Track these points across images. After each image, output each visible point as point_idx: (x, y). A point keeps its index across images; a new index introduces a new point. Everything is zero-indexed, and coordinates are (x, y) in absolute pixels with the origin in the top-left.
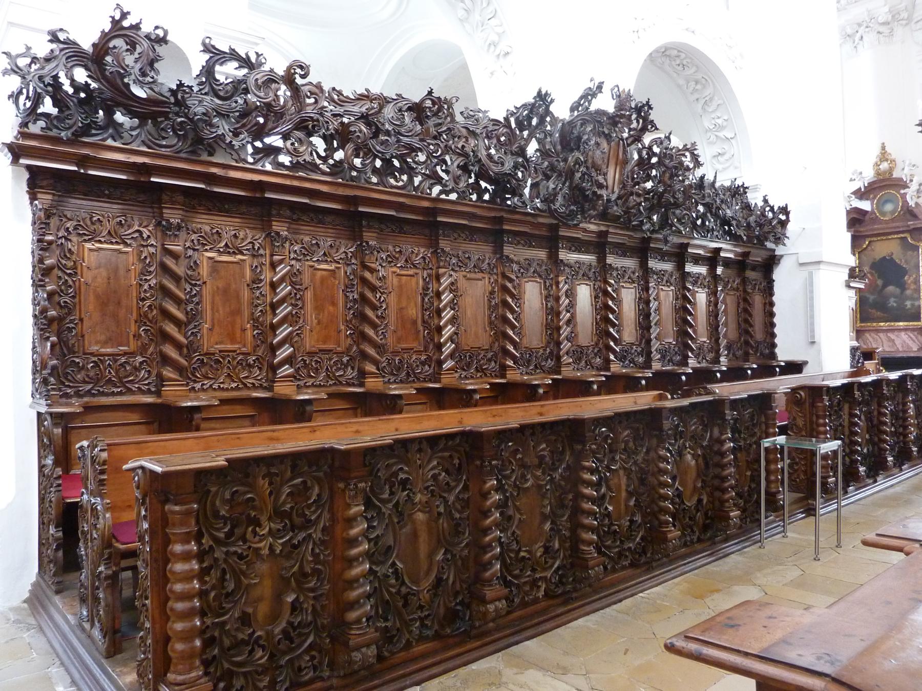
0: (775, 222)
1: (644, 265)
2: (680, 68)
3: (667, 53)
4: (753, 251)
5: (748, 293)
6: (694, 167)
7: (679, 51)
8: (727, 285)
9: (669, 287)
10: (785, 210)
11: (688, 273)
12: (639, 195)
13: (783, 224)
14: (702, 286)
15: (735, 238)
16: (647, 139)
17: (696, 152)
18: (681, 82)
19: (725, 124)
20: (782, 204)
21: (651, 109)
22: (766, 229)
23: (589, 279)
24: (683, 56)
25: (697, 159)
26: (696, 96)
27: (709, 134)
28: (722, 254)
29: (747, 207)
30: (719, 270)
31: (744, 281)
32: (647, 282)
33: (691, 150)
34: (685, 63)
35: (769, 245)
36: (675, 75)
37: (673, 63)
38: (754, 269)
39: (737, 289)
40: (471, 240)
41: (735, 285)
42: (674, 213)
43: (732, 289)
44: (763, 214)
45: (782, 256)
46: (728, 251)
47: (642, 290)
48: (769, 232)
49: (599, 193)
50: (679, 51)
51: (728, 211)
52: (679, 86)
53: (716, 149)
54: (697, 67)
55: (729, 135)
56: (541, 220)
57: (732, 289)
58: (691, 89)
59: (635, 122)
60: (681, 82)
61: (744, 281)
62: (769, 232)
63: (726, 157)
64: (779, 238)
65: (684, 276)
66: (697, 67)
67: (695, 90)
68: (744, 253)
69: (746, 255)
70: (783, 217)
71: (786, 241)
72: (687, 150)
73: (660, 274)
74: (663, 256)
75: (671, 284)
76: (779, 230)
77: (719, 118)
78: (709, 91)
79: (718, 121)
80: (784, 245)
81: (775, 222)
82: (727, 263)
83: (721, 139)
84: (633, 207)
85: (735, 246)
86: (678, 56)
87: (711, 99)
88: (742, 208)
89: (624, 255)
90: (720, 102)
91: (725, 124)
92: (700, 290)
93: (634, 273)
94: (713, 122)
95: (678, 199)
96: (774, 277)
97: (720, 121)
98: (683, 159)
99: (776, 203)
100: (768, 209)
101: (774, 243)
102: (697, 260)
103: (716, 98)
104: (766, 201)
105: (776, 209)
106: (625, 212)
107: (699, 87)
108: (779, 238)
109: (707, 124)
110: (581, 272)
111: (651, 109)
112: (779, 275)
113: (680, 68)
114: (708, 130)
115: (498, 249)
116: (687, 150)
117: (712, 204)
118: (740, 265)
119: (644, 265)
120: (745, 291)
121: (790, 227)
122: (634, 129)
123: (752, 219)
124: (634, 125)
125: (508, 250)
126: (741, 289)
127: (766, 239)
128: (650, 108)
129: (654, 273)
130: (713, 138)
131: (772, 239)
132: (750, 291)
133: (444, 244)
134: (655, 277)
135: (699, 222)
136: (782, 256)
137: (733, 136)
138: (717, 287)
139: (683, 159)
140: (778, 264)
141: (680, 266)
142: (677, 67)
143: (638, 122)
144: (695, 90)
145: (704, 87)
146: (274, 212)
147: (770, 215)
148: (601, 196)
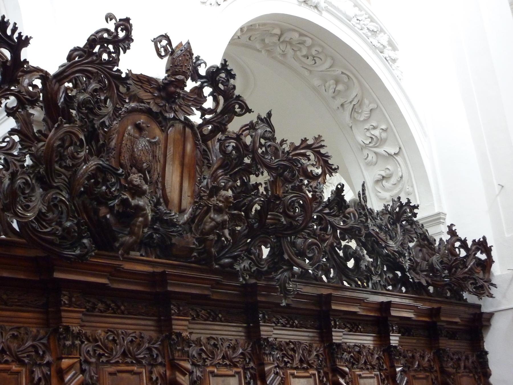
0: (471, 264)
1: (253, 334)
2: (310, 62)
3: (287, 37)
4: (443, 307)
5: (449, 375)
6: (324, 174)
7: (301, 35)
8: (413, 364)
9: (306, 370)
10: (482, 245)
11: (339, 345)
12: (219, 210)
13: (486, 265)
14: (368, 366)
15: (417, 290)
16: (235, 125)
17: (323, 151)
18: (316, 82)
19: (384, 135)
20: (478, 237)
21: (233, 77)
22: (460, 273)
23: (139, 362)
24: (309, 42)
25: (326, 162)
26: (339, 101)
27: (366, 152)
28: (394, 313)
29: (425, 241)
30: (394, 340)
31: (440, 355)
32: (261, 364)
33: (316, 148)
34: (314, 53)
35: (469, 297)
36: (306, 73)
37: (298, 53)
38: (452, 335)
39: (430, 369)
40: (214, 320)
41: (425, 362)
42: (293, 244)
43: (421, 368)
44: (452, 251)
45: (491, 315)
46: (404, 306)
47: (253, 377)
48: (465, 279)
49: (134, 202)
50: (301, 35)
51: (391, 243)
52: (315, 89)
53: (378, 172)
54: (333, 59)
55: (392, 151)
56: (20, 252)
57: (421, 368)
58: (331, 91)
59: (210, 99)
60: (316, 82)
61: (440, 355)
62: (465, 279)
63: (393, 180)
64: (482, 287)
65: (333, 350)
66: (333, 59)
67: (336, 93)
68: (432, 309)
69: (434, 313)
70: (483, 257)
71: (493, 290)
72: (309, 147)
73: (287, 349)
74: (291, 317)
75: (311, 366)
76: (481, 275)
77: (374, 128)
78: (355, 91)
79: (374, 132)
80: (491, 296)
81: (471, 264)
82: (406, 327)
83: (383, 156)
84: (211, 231)
85: (415, 299)
86: (303, 43)
87: (360, 103)
88: (419, 245)
89: (213, 317)
90: (372, 106)
91: (384, 135)
92: (365, 373)
93: (234, 349)
94: (368, 134)
95: (293, 218)
96: (487, 347)
97: (376, 132)
98: (304, 161)
99: (469, 234)
100: (457, 244)
101: (475, 294)
102: (354, 323)
103: (366, 101)
104: (452, 232)
105: (470, 243)
106: (201, 241)
107: (340, 87)
108: (482, 287)
109: (361, 138)
110: (118, 350)
111: (233, 77)
112: (494, 342)
113: (310, 62)
114: (363, 147)
115: (164, 325)
116: (309, 147)
117: (360, 230)
118: (427, 330)
119: (253, 334)
120: (443, 371)
121: (496, 269)
122: (209, 111)
123: (435, 259)
124: (209, 104)
125: (181, 325)
126: (436, 368)
127: (464, 289)
128: (231, 75)
129: (272, 346)
130: (372, 157)
131: (471, 288)
132: (450, 370)
133: (72, 319)
134: (277, 354)
135: (351, 264)
136: (491, 315)
137: (397, 151)
138: (393, 367)
139: (304, 161)
140: (488, 326)
141: (325, 336)
142: (304, 60)
143: (216, 100)
144: (336, 93)
145: (348, 88)
146: (65, 300)
147: (463, 253)
148: (139, 209)
